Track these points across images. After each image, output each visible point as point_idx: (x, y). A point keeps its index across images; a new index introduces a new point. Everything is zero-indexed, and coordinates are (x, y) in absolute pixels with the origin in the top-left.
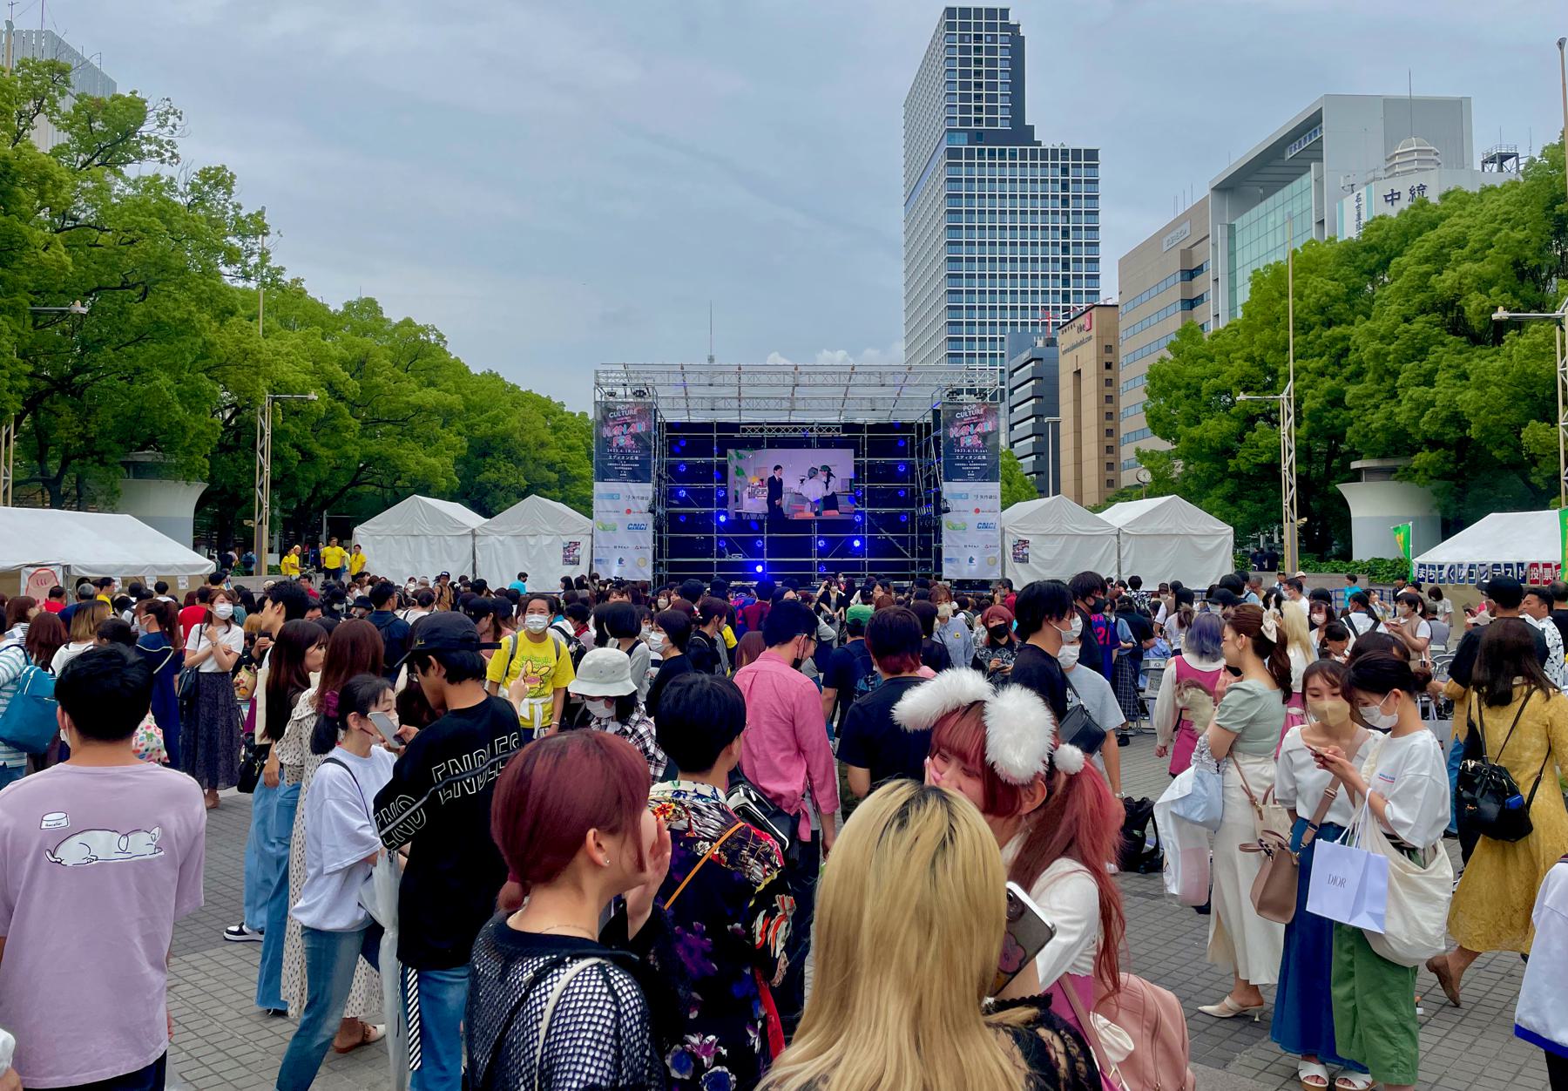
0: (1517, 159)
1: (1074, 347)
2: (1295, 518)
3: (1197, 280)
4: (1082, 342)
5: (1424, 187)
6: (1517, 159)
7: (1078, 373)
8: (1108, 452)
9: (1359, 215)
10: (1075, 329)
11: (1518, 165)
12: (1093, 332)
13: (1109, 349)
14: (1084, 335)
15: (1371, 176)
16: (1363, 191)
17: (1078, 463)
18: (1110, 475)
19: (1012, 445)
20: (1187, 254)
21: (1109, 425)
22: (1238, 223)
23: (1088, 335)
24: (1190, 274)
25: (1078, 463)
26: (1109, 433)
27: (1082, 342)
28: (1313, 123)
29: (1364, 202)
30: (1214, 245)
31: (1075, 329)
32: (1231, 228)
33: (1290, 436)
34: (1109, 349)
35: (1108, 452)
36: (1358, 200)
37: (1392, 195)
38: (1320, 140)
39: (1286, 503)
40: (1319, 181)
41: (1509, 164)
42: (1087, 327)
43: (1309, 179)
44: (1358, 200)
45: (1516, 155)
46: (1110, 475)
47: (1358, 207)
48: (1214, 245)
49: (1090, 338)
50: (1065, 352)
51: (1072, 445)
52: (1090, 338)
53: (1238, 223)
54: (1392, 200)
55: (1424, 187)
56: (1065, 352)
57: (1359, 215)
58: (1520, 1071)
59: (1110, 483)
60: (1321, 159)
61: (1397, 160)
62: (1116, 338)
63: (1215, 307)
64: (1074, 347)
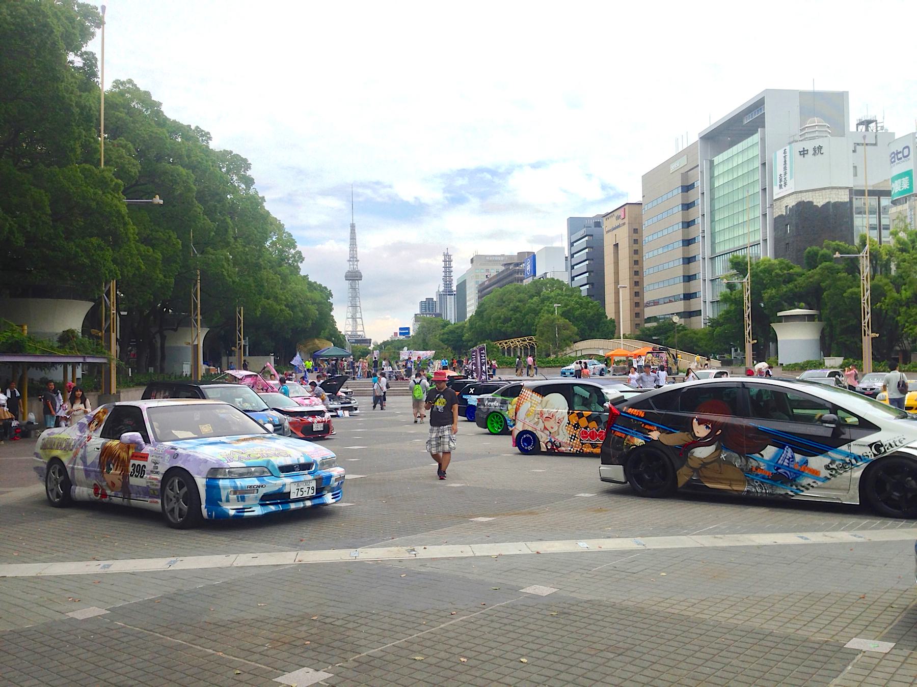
0: (876, 123)
1: (614, 229)
2: (751, 340)
3: (691, 192)
4: (619, 226)
5: (821, 147)
6: (876, 123)
7: (616, 245)
8: (636, 296)
9: (785, 161)
10: (614, 218)
11: (877, 127)
12: (626, 220)
13: (636, 231)
14: (620, 222)
15: (792, 140)
16: (788, 148)
17: (617, 273)
18: (637, 310)
19: (573, 279)
20: (685, 175)
21: (636, 278)
22: (717, 160)
23: (620, 222)
24: (687, 188)
25: (617, 273)
26: (636, 252)
27: (619, 226)
28: (758, 105)
29: (788, 154)
30: (702, 172)
31: (614, 218)
32: (712, 162)
33: (748, 299)
34: (636, 231)
35: (636, 296)
36: (785, 152)
37: (804, 151)
38: (764, 113)
39: (746, 333)
40: (763, 140)
41: (872, 125)
42: (622, 217)
43: (756, 138)
44: (785, 152)
45: (876, 121)
46: (637, 310)
47: (785, 157)
48: (702, 172)
49: (624, 224)
50: (607, 232)
51: (612, 271)
52: (624, 224)
53: (717, 160)
54: (804, 154)
55: (821, 147)
56: (607, 232)
57: (785, 161)
58: (906, 659)
59: (637, 315)
60: (764, 127)
61: (806, 130)
62: (641, 224)
63: (703, 209)
64: (614, 229)
